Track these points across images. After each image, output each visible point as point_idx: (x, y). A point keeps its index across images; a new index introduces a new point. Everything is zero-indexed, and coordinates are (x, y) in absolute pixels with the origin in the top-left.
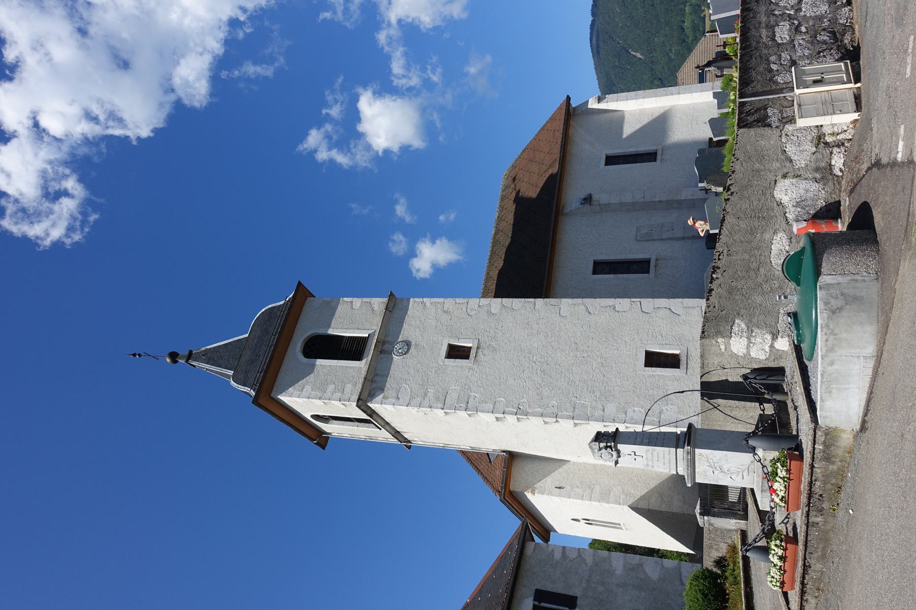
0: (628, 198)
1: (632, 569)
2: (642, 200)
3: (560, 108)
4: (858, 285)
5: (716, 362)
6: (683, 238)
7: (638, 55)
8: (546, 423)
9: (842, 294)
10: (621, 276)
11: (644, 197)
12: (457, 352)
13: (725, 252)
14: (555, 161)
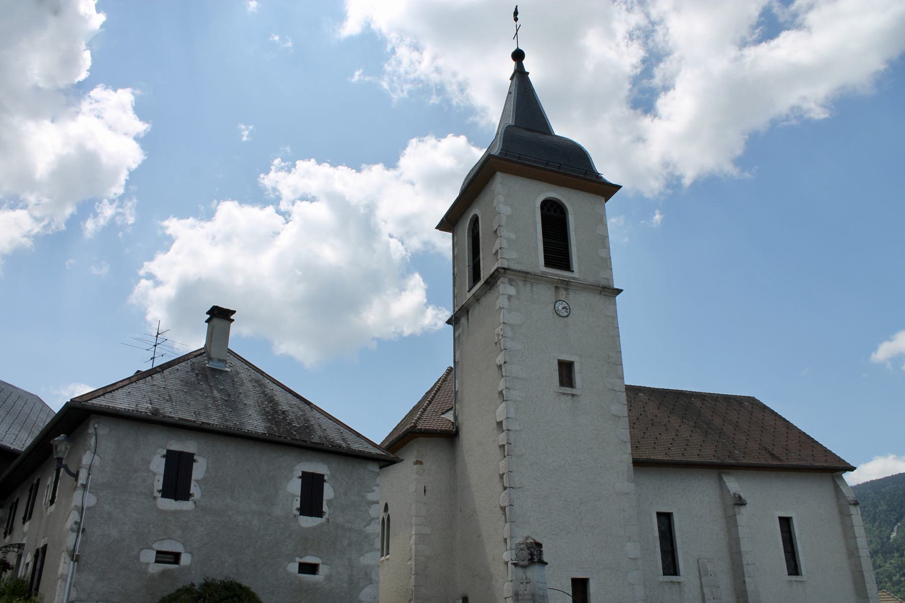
0: (745, 547)
1: (366, 574)
2: (744, 562)
3: (840, 460)
7: (894, 535)
8: (502, 476)
10: (658, 544)
11: (748, 564)
12: (566, 371)
14: (779, 459)
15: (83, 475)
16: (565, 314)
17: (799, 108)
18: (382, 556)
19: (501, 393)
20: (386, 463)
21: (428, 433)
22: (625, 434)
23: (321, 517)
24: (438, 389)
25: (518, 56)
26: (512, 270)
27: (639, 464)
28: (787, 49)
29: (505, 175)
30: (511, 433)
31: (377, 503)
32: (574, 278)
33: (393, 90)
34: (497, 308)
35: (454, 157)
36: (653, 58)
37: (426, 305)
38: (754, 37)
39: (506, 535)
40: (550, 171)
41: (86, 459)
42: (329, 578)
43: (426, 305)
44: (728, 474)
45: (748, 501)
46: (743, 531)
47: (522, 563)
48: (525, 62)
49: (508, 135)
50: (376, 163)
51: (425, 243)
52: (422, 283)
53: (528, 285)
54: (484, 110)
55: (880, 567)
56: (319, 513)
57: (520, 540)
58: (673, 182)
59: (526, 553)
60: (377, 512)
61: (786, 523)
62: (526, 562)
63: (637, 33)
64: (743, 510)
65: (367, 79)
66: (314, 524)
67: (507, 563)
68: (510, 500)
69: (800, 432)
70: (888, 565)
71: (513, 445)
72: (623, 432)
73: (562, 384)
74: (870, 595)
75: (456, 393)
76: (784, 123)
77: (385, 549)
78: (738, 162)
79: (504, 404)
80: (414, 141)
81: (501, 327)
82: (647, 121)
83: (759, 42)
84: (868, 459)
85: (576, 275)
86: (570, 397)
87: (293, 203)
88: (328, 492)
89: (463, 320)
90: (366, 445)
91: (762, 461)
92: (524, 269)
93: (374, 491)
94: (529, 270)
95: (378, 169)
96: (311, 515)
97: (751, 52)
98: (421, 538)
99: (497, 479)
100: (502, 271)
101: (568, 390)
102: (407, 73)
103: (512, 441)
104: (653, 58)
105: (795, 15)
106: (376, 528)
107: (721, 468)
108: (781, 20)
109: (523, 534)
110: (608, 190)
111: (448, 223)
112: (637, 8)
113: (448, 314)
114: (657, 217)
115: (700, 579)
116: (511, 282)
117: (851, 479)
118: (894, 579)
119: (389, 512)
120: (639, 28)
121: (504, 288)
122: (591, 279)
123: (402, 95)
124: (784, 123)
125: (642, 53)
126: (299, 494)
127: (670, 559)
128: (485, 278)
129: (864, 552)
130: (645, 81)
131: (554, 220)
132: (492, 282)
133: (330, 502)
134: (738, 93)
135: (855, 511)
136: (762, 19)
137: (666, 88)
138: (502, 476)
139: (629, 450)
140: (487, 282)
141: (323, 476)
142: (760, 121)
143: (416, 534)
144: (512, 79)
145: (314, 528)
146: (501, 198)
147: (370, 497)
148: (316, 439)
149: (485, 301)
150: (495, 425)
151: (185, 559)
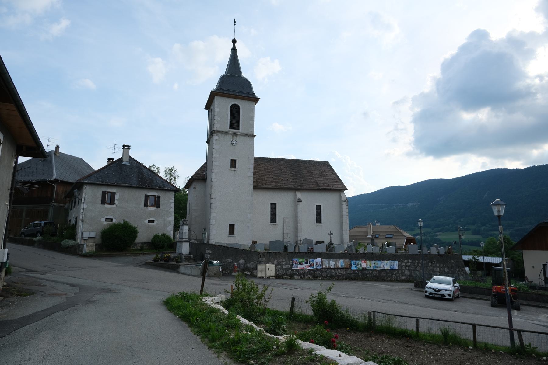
0: (299, 214)
12: (233, 163)
15: (83, 200)
25: (234, 41)
41: (84, 195)
42: (157, 224)
49: (223, 80)
64: (300, 203)
73: (232, 167)
101: (234, 169)
122: (245, 132)
131: (235, 112)
151: (114, 220)
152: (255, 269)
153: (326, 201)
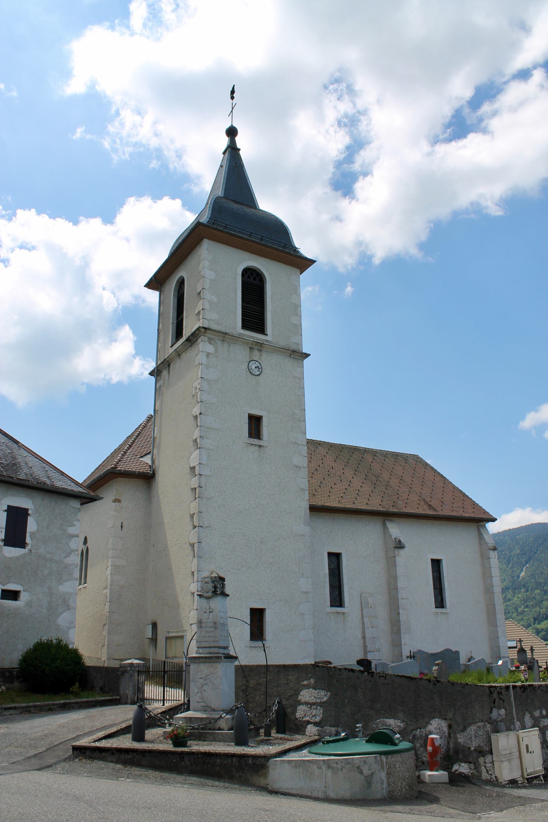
0: (401, 584)
2: (400, 597)
3: (485, 512)
4: (380, 784)
5: (290, 678)
6: (364, 638)
7: (523, 574)
8: (192, 516)
9: (372, 774)
11: (403, 599)
12: (255, 424)
13: (386, 681)
14: (435, 510)
16: (257, 373)
17: (478, 204)
18: (80, 584)
19: (195, 441)
20: (87, 500)
21: (126, 475)
22: (304, 484)
23: (24, 547)
24: (139, 435)
25: (232, 132)
26: (212, 330)
27: (314, 509)
28: (472, 151)
29: (211, 242)
30: (203, 477)
31: (77, 536)
32: (267, 341)
33: (116, 151)
34: (196, 363)
35: (173, 218)
36: (356, 146)
37: (134, 357)
38: (446, 135)
39: (194, 569)
40: (253, 241)
42: (29, 604)
43: (134, 357)
44: (391, 521)
45: (406, 545)
46: (400, 571)
47: (206, 595)
48: (237, 139)
49: (217, 206)
50: (94, 216)
51: (137, 297)
52: (132, 335)
53: (226, 345)
54: (199, 177)
55: (509, 600)
56: (22, 544)
57: (206, 574)
58: (365, 259)
59: (210, 586)
60: (77, 545)
61: (436, 564)
62: (210, 594)
63: (345, 120)
64: (402, 552)
65: (89, 137)
66: (22, 553)
67: (193, 594)
68: (199, 537)
69: (454, 487)
70: (515, 599)
71: (204, 488)
72: (302, 480)
73: (251, 435)
74: (498, 624)
75: (154, 439)
76: (464, 216)
77: (83, 578)
78: (422, 246)
79: (197, 451)
80: (132, 200)
81: (199, 381)
82: (345, 203)
83: (449, 140)
84: (509, 510)
85: (269, 338)
86: (257, 448)
87: (13, 250)
88: (32, 525)
89: (165, 373)
90: (69, 482)
91: (421, 511)
92: (223, 329)
93: (74, 525)
94: (227, 331)
95: (96, 223)
96: (14, 546)
97: (442, 149)
98: (116, 569)
99: (188, 518)
100: (203, 330)
101: (256, 441)
102: (129, 136)
103: (203, 485)
104: (356, 146)
105: (481, 120)
106: (75, 559)
107: (385, 516)
108: (469, 122)
109: (212, 568)
110: (303, 263)
111: (156, 282)
112: (346, 97)
113: (152, 365)
114: (349, 289)
115: (362, 610)
116: (210, 340)
117: (492, 528)
118: (520, 610)
119: (88, 545)
120: (346, 116)
121: (203, 346)
123: (124, 158)
124: (464, 216)
125: (347, 140)
126: (4, 526)
127: (337, 593)
128: (187, 336)
129: (497, 590)
130: (346, 166)
131: (253, 288)
132: (192, 340)
133: (32, 534)
134: (427, 185)
135: (493, 555)
136: (454, 120)
137: (365, 174)
138: (192, 516)
139: (307, 497)
140: (188, 340)
141: (27, 510)
142: (443, 212)
143: (112, 565)
144: (224, 153)
145: (17, 558)
146: (206, 263)
147: (71, 530)
148: (22, 476)
149: (184, 356)
150: (188, 470)
152: (486, 750)
153: (452, 547)
